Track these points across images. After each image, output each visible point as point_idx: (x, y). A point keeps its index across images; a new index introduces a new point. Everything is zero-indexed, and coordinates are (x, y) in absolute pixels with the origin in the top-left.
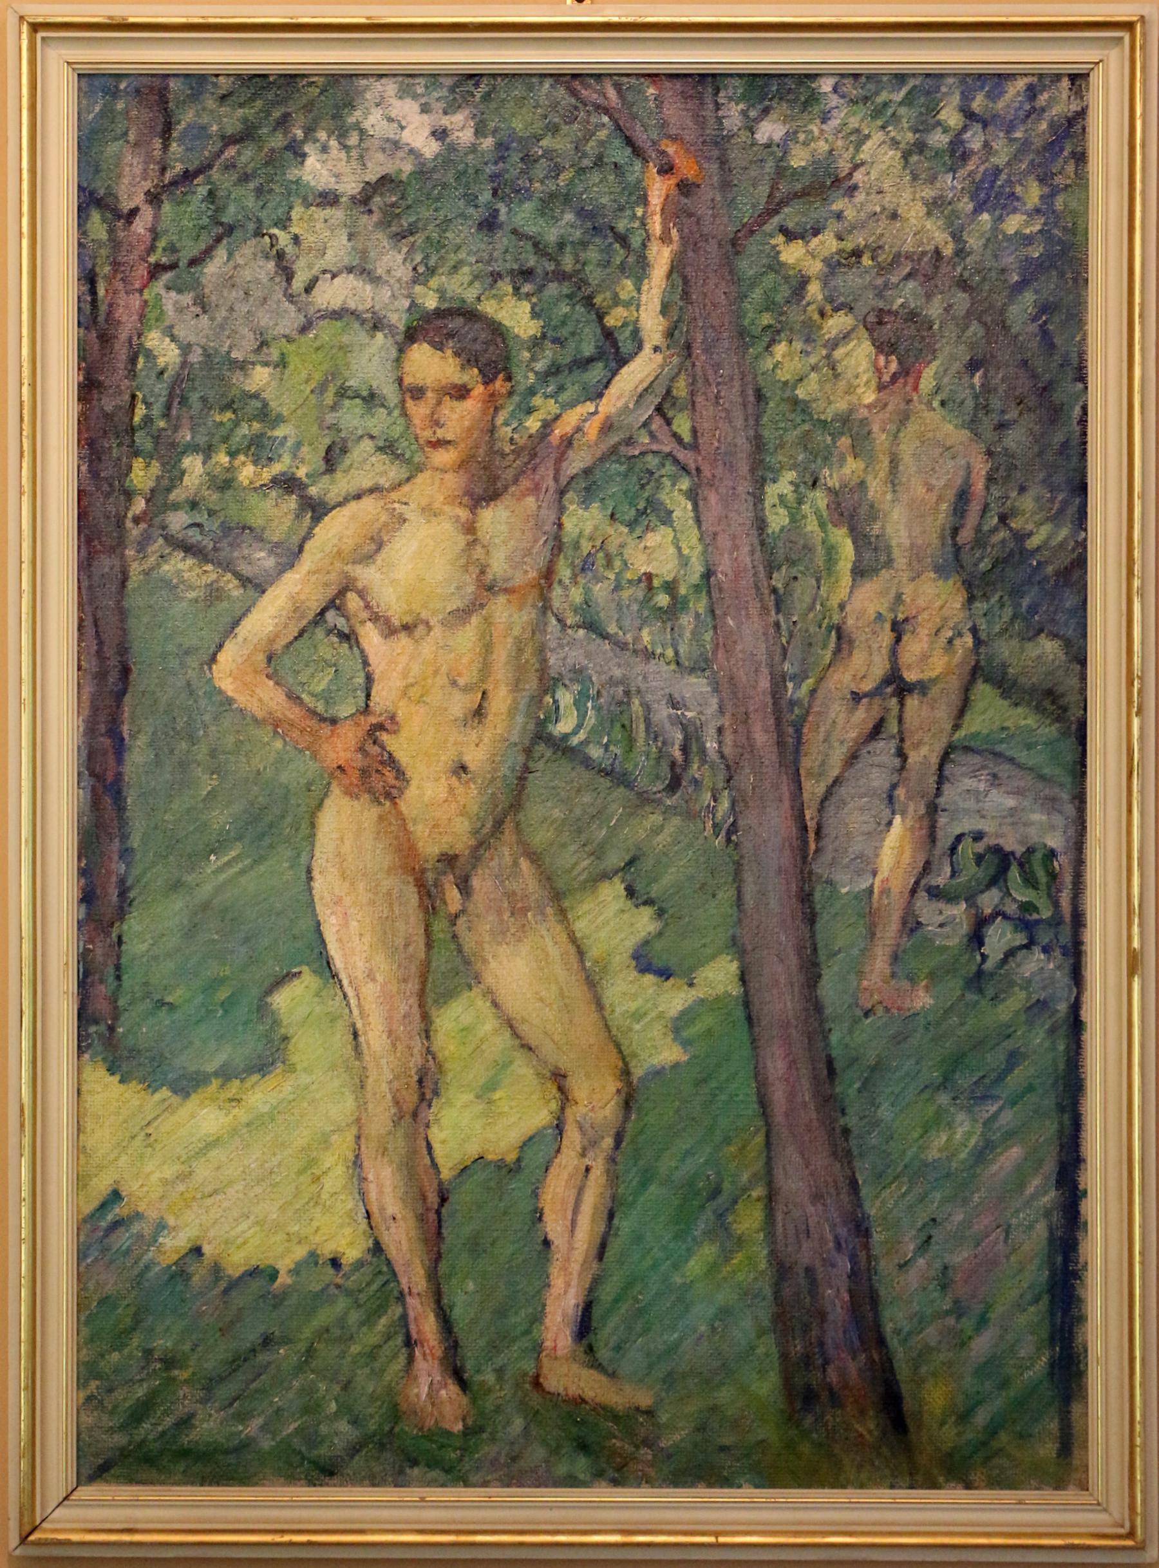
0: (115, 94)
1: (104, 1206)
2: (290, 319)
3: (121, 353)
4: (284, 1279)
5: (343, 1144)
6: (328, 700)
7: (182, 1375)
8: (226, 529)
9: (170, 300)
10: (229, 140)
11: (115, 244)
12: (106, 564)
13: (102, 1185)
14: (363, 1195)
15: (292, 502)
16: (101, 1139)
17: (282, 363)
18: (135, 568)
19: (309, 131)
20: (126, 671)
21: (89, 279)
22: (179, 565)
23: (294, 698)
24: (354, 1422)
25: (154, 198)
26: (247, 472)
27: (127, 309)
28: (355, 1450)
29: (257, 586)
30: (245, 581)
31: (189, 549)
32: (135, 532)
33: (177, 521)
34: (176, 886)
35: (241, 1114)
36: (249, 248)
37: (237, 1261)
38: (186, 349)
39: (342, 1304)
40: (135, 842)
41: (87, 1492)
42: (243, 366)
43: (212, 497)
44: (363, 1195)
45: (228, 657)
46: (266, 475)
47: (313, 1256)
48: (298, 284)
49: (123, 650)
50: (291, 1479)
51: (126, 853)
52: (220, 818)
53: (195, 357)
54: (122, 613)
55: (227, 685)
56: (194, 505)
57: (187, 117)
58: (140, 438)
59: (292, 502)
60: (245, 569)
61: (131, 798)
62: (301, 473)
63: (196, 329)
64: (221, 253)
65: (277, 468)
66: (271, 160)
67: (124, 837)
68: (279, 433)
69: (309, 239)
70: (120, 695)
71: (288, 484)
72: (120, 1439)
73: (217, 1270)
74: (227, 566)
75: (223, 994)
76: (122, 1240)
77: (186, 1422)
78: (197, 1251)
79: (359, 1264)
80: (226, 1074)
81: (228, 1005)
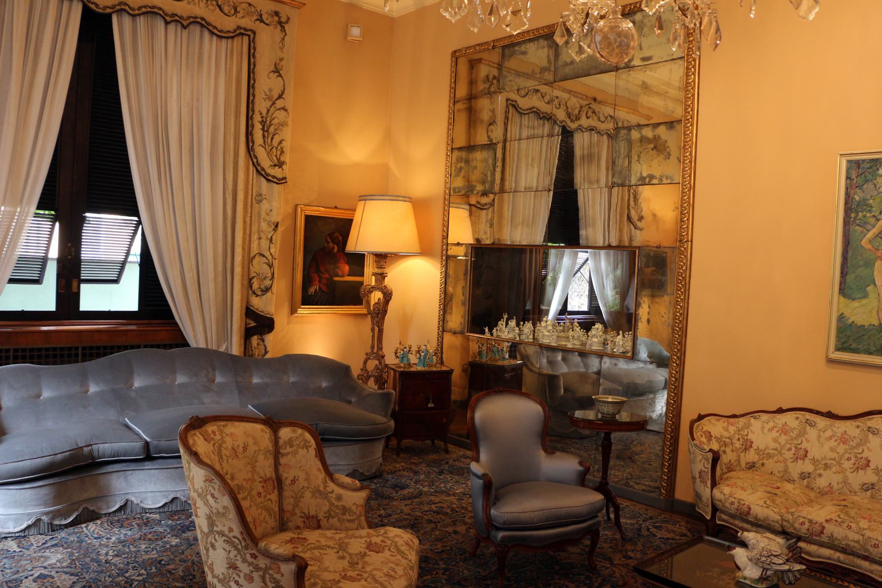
0: (852, 163)
1: (841, 315)
2: (876, 193)
3: (851, 198)
4: (866, 327)
5: (876, 309)
6: (878, 247)
7: (850, 338)
8: (865, 223)
9: (858, 191)
10: (868, 168)
11: (851, 184)
12: (847, 228)
13: (841, 312)
14: (879, 317)
15: (875, 219)
16: (841, 306)
17: (874, 199)
18: (851, 229)
19: (880, 166)
20: (849, 243)
21: (847, 189)
22: (857, 228)
23: (873, 246)
24: (876, 347)
25: (857, 177)
26: (868, 215)
27: (852, 192)
28: (875, 351)
29: (869, 231)
30: (867, 230)
31: (859, 225)
32: (851, 223)
33: (858, 222)
34: (854, 272)
35: (861, 304)
36: (870, 183)
37: (859, 324)
38: (860, 197)
39: (874, 331)
40: (849, 266)
41: (836, 352)
42: (868, 200)
43: (863, 218)
44: (879, 317)
45: (863, 241)
46: (871, 215)
47: (871, 324)
48: (877, 188)
49: (848, 239)
50: (865, 354)
51: (847, 268)
52: (861, 263)
53: (862, 199)
54: (849, 235)
55: (863, 244)
56: (860, 219)
57: (862, 166)
58: (853, 210)
59: (875, 219)
60: (867, 228)
61: (848, 260)
62: (876, 215)
63: (861, 195)
64: (866, 184)
65: (872, 214)
66: (874, 171)
67: (847, 265)
68: (873, 209)
69: (879, 182)
70: (848, 246)
71: (874, 216)
72: (841, 346)
73: (856, 325)
74: (864, 228)
75: (859, 287)
76: (843, 320)
77: (851, 345)
78: (853, 322)
79: (877, 326)
80: (859, 298)
81: (861, 289)
